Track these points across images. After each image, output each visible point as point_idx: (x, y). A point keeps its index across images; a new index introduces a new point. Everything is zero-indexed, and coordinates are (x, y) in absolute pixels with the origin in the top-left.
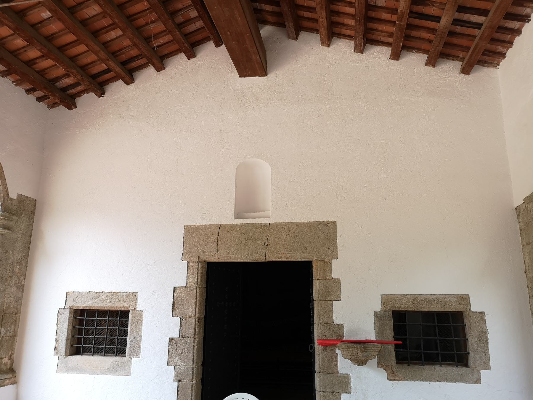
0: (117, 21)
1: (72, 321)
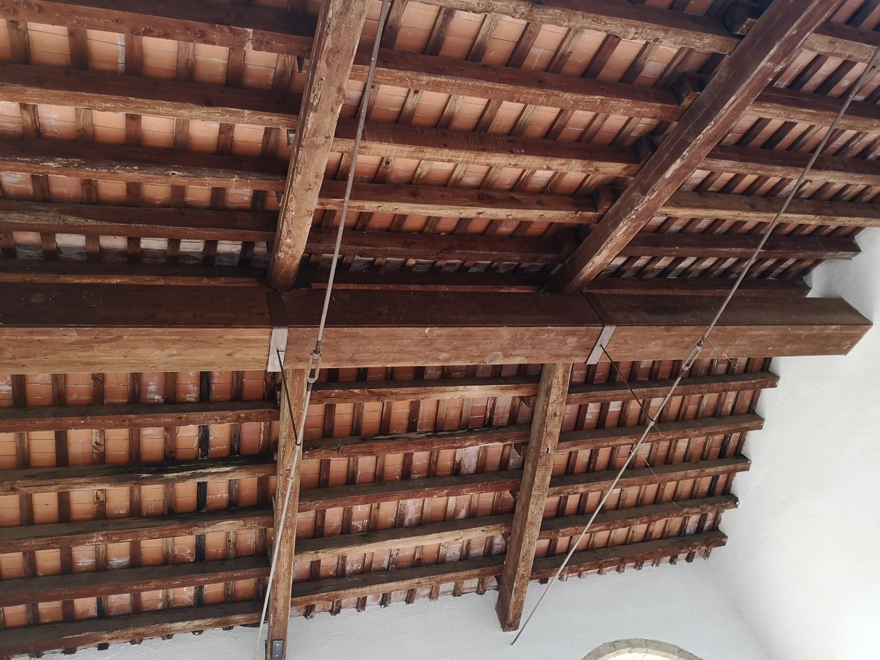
0: (671, 437)
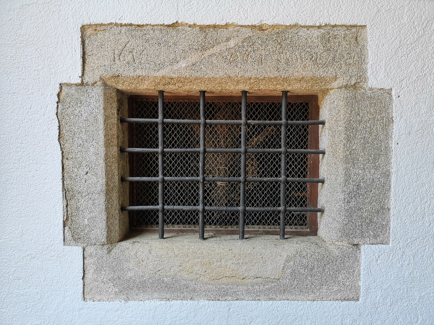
1: (115, 131)
